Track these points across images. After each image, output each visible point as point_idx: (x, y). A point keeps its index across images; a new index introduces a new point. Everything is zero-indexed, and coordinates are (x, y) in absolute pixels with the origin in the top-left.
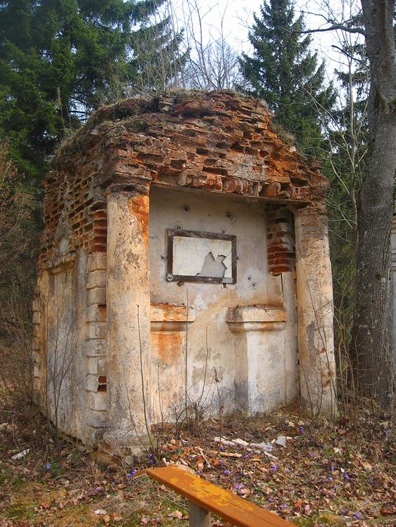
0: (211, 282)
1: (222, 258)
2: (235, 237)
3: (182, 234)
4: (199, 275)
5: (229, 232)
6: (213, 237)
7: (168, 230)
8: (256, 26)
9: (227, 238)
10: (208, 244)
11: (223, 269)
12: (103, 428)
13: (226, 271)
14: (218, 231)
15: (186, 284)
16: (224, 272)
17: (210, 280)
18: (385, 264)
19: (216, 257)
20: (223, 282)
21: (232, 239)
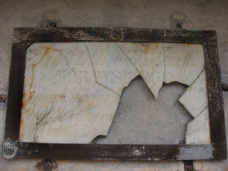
0: (140, 160)
1: (175, 90)
2: (212, 33)
3: (52, 35)
4: (101, 142)
5: (194, 23)
6: (149, 37)
7: (21, 30)
8: (40, 161)
9: (182, 37)
10: (131, 55)
11: (183, 120)
12: (42, 160)
13: (192, 126)
14: (161, 22)
15: (86, 140)
16: (186, 126)
17: (137, 152)
18: (40, 169)
19: (155, 87)
20: (181, 157)
21: (205, 38)
